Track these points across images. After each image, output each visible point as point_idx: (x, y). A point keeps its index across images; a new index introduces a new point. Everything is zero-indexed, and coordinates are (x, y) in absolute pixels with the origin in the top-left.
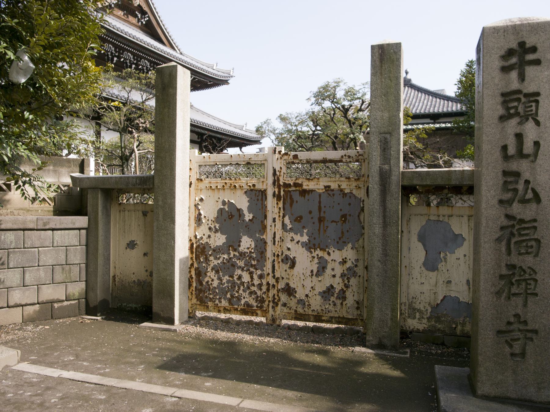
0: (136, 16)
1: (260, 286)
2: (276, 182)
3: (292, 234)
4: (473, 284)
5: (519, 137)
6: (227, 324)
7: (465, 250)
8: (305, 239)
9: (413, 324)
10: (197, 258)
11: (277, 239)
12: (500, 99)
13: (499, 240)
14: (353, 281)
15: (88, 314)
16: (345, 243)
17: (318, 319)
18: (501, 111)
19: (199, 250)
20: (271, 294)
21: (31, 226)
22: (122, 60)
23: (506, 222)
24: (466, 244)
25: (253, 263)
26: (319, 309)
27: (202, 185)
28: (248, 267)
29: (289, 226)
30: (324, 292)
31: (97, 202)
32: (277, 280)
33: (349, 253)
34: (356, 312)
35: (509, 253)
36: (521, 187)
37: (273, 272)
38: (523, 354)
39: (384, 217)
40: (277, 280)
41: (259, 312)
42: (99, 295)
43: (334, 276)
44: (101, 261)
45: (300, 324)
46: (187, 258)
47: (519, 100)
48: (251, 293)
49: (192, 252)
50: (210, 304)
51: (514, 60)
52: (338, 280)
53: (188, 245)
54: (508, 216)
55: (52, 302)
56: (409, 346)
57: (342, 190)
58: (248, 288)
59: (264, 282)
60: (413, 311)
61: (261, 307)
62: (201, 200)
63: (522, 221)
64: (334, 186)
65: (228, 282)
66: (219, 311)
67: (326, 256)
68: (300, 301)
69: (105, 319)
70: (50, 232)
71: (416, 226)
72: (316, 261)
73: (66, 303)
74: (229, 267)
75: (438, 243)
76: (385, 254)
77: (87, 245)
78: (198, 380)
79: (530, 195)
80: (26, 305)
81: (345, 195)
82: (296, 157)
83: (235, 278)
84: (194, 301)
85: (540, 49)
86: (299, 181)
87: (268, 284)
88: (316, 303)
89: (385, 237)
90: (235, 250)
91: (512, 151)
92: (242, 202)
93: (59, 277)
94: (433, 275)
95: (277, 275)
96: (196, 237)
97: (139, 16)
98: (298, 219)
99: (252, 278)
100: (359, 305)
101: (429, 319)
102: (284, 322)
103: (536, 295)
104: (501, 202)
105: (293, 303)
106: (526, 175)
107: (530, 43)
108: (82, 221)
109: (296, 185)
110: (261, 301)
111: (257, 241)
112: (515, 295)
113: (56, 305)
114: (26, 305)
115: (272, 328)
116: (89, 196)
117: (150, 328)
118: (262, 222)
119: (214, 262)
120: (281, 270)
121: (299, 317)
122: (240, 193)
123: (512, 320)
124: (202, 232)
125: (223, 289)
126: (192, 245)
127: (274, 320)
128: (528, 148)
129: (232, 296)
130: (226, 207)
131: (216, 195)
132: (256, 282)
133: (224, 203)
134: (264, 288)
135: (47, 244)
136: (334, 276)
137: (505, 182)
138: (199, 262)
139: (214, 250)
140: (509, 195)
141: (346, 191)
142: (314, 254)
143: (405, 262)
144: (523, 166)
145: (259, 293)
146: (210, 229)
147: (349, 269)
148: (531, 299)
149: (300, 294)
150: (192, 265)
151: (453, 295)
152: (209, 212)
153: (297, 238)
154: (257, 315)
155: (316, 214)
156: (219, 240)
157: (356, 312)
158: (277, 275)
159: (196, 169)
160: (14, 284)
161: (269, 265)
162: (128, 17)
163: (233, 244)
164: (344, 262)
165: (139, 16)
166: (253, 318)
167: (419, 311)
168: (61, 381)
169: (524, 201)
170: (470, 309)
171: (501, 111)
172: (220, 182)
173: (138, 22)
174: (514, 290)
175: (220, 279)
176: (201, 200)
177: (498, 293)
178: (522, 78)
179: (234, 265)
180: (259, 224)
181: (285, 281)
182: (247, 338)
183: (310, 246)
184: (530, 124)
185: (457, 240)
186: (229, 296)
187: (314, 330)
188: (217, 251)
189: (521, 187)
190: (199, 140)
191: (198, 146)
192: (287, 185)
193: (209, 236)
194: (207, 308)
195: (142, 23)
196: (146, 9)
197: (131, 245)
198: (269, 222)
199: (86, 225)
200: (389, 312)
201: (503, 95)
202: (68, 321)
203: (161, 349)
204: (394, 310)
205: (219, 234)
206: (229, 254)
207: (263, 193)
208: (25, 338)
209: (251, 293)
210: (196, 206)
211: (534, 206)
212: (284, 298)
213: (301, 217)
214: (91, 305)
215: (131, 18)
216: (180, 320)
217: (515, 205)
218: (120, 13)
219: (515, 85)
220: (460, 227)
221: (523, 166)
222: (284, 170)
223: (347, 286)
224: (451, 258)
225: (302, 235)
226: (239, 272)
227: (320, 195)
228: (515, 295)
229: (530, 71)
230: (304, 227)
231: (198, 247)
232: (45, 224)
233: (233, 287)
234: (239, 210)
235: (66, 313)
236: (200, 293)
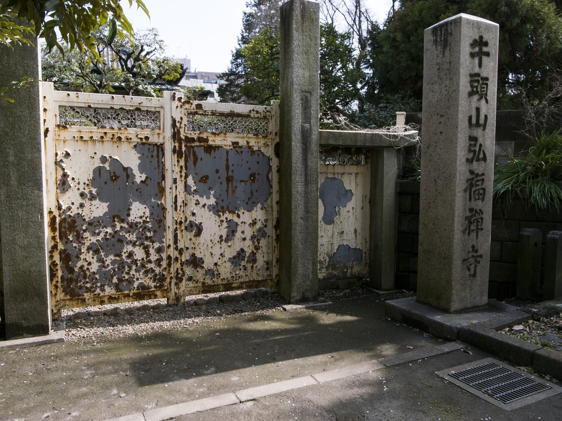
1: (158, 262)
2: (176, 136)
3: (197, 197)
11: (179, 203)
12: (469, 79)
16: (255, 204)
25: (148, 234)
26: (229, 275)
28: (142, 241)
29: (194, 188)
30: (234, 257)
41: (158, 293)
51: (477, 49)
52: (248, 242)
54: (471, 172)
57: (250, 147)
58: (143, 266)
63: (477, 175)
65: (113, 262)
67: (236, 219)
68: (210, 272)
85: (490, 45)
87: (169, 257)
98: (204, 179)
99: (148, 254)
104: (467, 160)
106: (480, 140)
119: (90, 239)
128: (482, 121)
134: (164, 264)
136: (244, 239)
137: (470, 145)
142: (223, 218)
145: (157, 270)
146: (82, 195)
149: (208, 263)
153: (203, 200)
163: (118, 214)
164: (254, 223)
175: (100, 260)
179: (121, 241)
180: (154, 187)
181: (191, 251)
183: (217, 209)
186: (115, 280)
192: (189, 140)
193: (82, 206)
206: (114, 226)
207: (160, 148)
212: (189, 271)
219: (477, 70)
223: (257, 248)
225: (208, 198)
226: (130, 248)
227: (227, 152)
230: (210, 189)
231: (63, 221)
234: (126, 170)
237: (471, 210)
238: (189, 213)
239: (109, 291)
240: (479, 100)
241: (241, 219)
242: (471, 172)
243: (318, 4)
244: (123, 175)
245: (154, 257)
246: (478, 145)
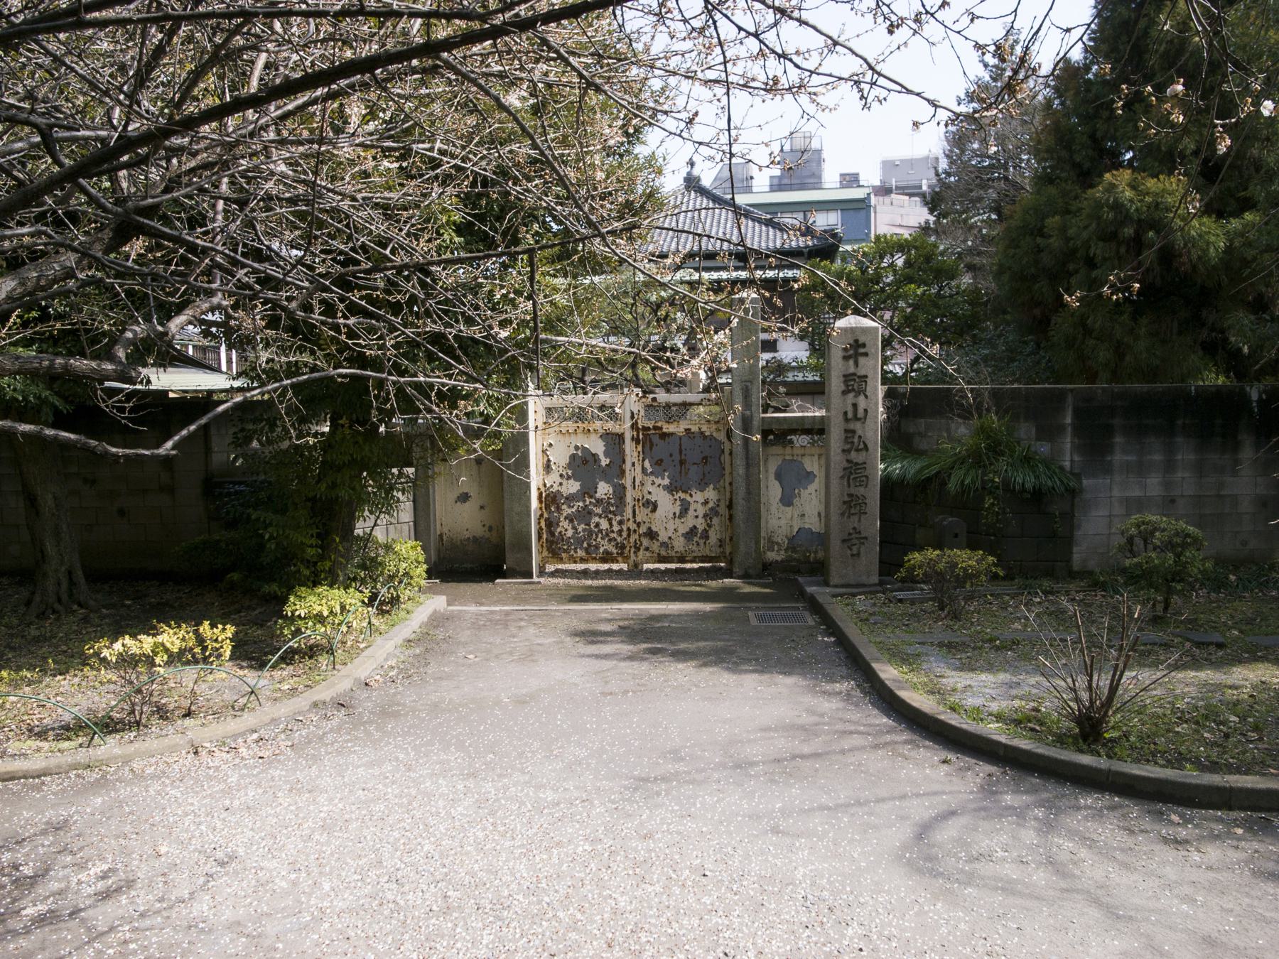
1: (620, 532)
2: (634, 426)
3: (653, 478)
4: (825, 516)
5: (855, 406)
6: (585, 574)
7: (816, 487)
8: (666, 482)
9: (772, 556)
10: (547, 507)
11: (637, 483)
12: (842, 379)
13: (842, 477)
14: (715, 521)
16: (707, 485)
17: (682, 560)
18: (843, 388)
20: (632, 540)
23: (846, 465)
24: (817, 480)
28: (606, 514)
29: (650, 470)
32: (639, 525)
33: (711, 494)
34: (719, 550)
35: (849, 486)
36: (856, 440)
37: (634, 517)
38: (858, 554)
39: (747, 458)
40: (639, 525)
41: (620, 559)
45: (662, 566)
48: (610, 540)
50: (564, 555)
52: (701, 520)
56: (769, 575)
58: (607, 535)
59: (625, 528)
60: (771, 544)
61: (622, 554)
63: (857, 464)
64: (694, 429)
65: (584, 530)
66: (575, 562)
67: (688, 498)
68: (664, 544)
71: (772, 468)
72: (678, 503)
74: (585, 515)
75: (793, 479)
76: (749, 492)
77: (414, 501)
79: (862, 446)
81: (705, 437)
84: (545, 553)
86: (659, 424)
87: (629, 529)
88: (679, 544)
89: (747, 476)
90: (591, 497)
91: (850, 415)
92: (597, 446)
94: (789, 509)
95: (638, 519)
96: (545, 485)
98: (658, 462)
99: (611, 525)
100: (721, 543)
101: (786, 550)
102: (646, 566)
104: (844, 451)
106: (860, 432)
107: (862, 340)
109: (655, 428)
111: (615, 486)
119: (567, 510)
121: (662, 560)
124: (552, 479)
127: (636, 565)
128: (861, 413)
129: (589, 545)
130: (579, 453)
131: (567, 439)
132: (616, 528)
134: (625, 534)
138: (550, 512)
139: (567, 498)
140: (848, 446)
143: (763, 500)
144: (857, 426)
145: (619, 539)
146: (561, 476)
147: (712, 509)
148: (863, 517)
149: (663, 537)
150: (542, 515)
151: (807, 526)
152: (560, 457)
153: (658, 481)
155: (677, 457)
156: (573, 487)
157: (719, 550)
158: (638, 519)
161: (629, 510)
164: (706, 502)
167: (778, 544)
169: (858, 450)
170: (822, 539)
171: (843, 388)
172: (570, 425)
174: (853, 511)
175: (574, 528)
176: (551, 445)
177: (842, 514)
178: (856, 364)
179: (590, 513)
180: (616, 469)
181: (648, 525)
183: (671, 489)
184: (862, 397)
185: (810, 476)
187: (677, 571)
188: (570, 499)
189: (856, 440)
192: (645, 429)
193: (561, 484)
194: (561, 560)
197: (464, 498)
198: (628, 466)
200: (753, 545)
201: (844, 376)
204: (757, 542)
205: (572, 481)
207: (621, 437)
209: (610, 540)
210: (544, 452)
211: (864, 453)
212: (646, 542)
213: (662, 460)
219: (852, 370)
220: (812, 465)
221: (857, 426)
222: (642, 413)
223: (709, 526)
224: (804, 493)
226: (597, 519)
229: (862, 360)
231: (547, 496)
234: (594, 456)
237: (850, 495)
239: (581, 553)
245: (616, 528)
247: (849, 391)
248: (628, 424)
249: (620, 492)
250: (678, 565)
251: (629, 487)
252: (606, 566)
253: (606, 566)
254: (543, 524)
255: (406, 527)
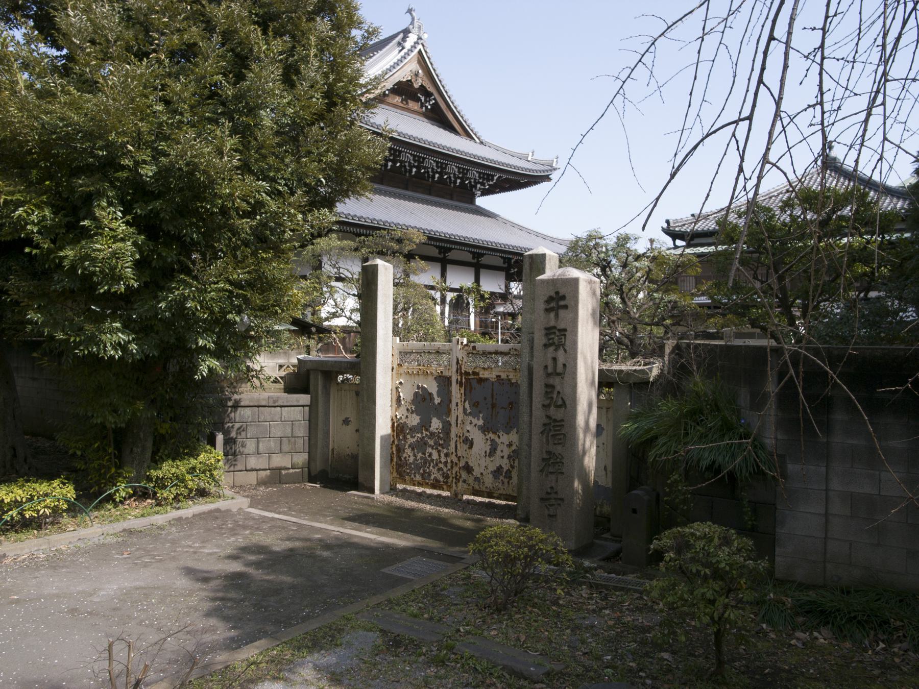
0: (419, 100)
1: (446, 463)
2: (459, 370)
3: (471, 418)
5: (555, 359)
10: (398, 436)
11: (459, 422)
12: (543, 332)
15: (310, 481)
16: (511, 428)
18: (544, 341)
19: (399, 428)
20: (454, 472)
21: (264, 403)
22: (398, 165)
25: (441, 442)
26: (490, 485)
27: (401, 370)
28: (437, 446)
29: (469, 411)
30: (495, 471)
31: (318, 382)
33: (514, 437)
36: (555, 396)
41: (445, 487)
42: (318, 466)
43: (502, 457)
44: (320, 435)
45: (479, 499)
46: (389, 435)
47: (555, 333)
49: (393, 431)
51: (553, 304)
52: (506, 461)
53: (390, 424)
54: (548, 417)
55: (280, 469)
57: (509, 380)
58: (437, 465)
61: (447, 482)
62: (401, 383)
63: (555, 421)
64: (504, 376)
65: (421, 458)
66: (414, 485)
67: (497, 439)
68: (476, 479)
69: (324, 487)
70: (279, 409)
73: (291, 471)
74: (421, 445)
78: (364, 527)
79: (560, 402)
80: (260, 470)
82: (474, 348)
83: (427, 455)
84: (395, 474)
85: (568, 298)
86: (477, 370)
87: (452, 462)
90: (427, 430)
92: (432, 387)
93: (286, 448)
97: (423, 99)
98: (475, 405)
99: (439, 455)
102: (465, 497)
103: (562, 473)
104: (544, 406)
105: (471, 480)
106: (558, 388)
107: (562, 293)
108: (305, 399)
109: (474, 373)
110: (446, 477)
112: (551, 473)
113: (283, 472)
114: (260, 470)
115: (454, 501)
116: (312, 377)
117: (355, 495)
118: (448, 406)
119: (411, 440)
120: (462, 449)
122: (431, 379)
123: (549, 491)
125: (417, 465)
126: (393, 424)
128: (560, 368)
129: (424, 471)
133: (418, 387)
134: (449, 466)
135: (276, 418)
136: (502, 457)
137: (546, 392)
138: (399, 440)
141: (513, 381)
142: (488, 437)
144: (556, 381)
145: (445, 469)
146: (408, 410)
149: (477, 472)
150: (393, 442)
152: (406, 395)
153: (475, 421)
154: (443, 490)
156: (414, 420)
159: (397, 356)
160: (251, 452)
161: (452, 448)
162: (407, 103)
163: (425, 424)
164: (510, 445)
165: (423, 99)
166: (439, 492)
168: (273, 519)
171: (544, 341)
173: (422, 107)
175: (415, 456)
176: (401, 383)
179: (426, 444)
180: (444, 410)
181: (465, 460)
182: (428, 507)
183: (484, 429)
186: (421, 471)
188: (413, 430)
190: (506, 265)
191: (504, 273)
192: (467, 373)
193: (407, 417)
194: (404, 482)
195: (426, 107)
196: (431, 89)
197: (346, 422)
199: (308, 403)
201: (546, 329)
202: (292, 486)
203: (353, 509)
205: (414, 415)
206: (422, 433)
207: (449, 379)
208: (257, 495)
210: (397, 388)
212: (464, 475)
214: (313, 474)
215: (412, 105)
216: (381, 490)
217: (552, 408)
218: (397, 100)
219: (552, 323)
221: (556, 381)
223: (513, 467)
225: (478, 419)
226: (429, 450)
227: (493, 383)
228: (551, 473)
229: (562, 313)
230: (480, 412)
231: (398, 425)
232: (274, 402)
233: (425, 463)
234: (430, 394)
235: (292, 479)
236: (399, 468)
237: (549, 453)
238: (465, 431)
239: (418, 478)
240: (556, 350)
241: (501, 440)
242: (548, 417)
243: (544, 255)
244: (428, 398)
245: (443, 460)
246: (556, 392)
247: (551, 345)
248: (454, 369)
249: (447, 427)
250: (487, 500)
251: (453, 425)
252: (436, 492)
253: (436, 492)
254: (394, 449)
255: (300, 441)
